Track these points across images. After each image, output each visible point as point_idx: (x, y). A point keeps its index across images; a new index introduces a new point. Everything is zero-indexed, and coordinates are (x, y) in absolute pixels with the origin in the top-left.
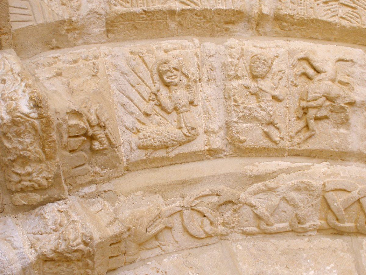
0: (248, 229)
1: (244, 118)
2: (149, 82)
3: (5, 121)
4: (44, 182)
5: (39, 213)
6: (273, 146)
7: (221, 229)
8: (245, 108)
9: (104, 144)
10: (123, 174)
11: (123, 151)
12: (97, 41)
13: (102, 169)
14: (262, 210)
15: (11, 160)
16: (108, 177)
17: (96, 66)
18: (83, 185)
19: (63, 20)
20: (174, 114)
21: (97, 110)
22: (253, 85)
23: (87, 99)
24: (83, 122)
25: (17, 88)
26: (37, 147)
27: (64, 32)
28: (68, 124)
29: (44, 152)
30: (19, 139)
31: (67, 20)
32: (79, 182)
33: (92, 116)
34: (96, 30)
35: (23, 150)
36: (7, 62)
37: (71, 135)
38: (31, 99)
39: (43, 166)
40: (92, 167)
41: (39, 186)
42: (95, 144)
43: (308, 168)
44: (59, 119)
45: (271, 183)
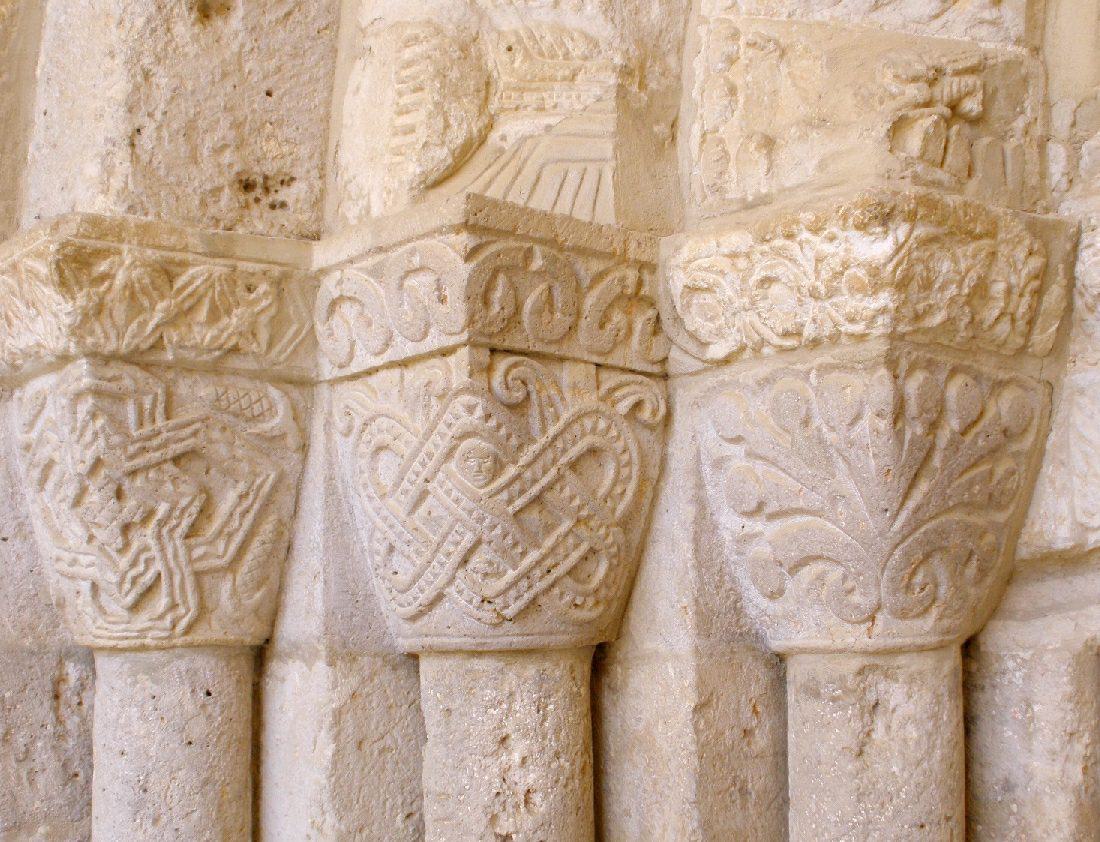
3: (891, 306)
4: (1036, 263)
5: (1090, 300)
9: (975, 86)
10: (1044, 63)
11: (991, 46)
12: (682, 18)
13: (1022, 112)
15: (970, 323)
16: (1043, 104)
17: (759, 41)
18: (1043, 175)
19: (618, 91)
21: (896, 76)
23: (862, 90)
24: (918, 118)
25: (810, 255)
26: (965, 248)
27: (644, 97)
28: (918, 158)
29: (979, 237)
30: (936, 286)
31: (620, 81)
32: (1033, 181)
33: (907, 92)
35: (960, 286)
36: (704, 262)
37: (939, 159)
38: (862, 227)
39: (1003, 250)
40: (1012, 136)
41: (1036, 277)
42: (968, 109)
44: (902, 175)
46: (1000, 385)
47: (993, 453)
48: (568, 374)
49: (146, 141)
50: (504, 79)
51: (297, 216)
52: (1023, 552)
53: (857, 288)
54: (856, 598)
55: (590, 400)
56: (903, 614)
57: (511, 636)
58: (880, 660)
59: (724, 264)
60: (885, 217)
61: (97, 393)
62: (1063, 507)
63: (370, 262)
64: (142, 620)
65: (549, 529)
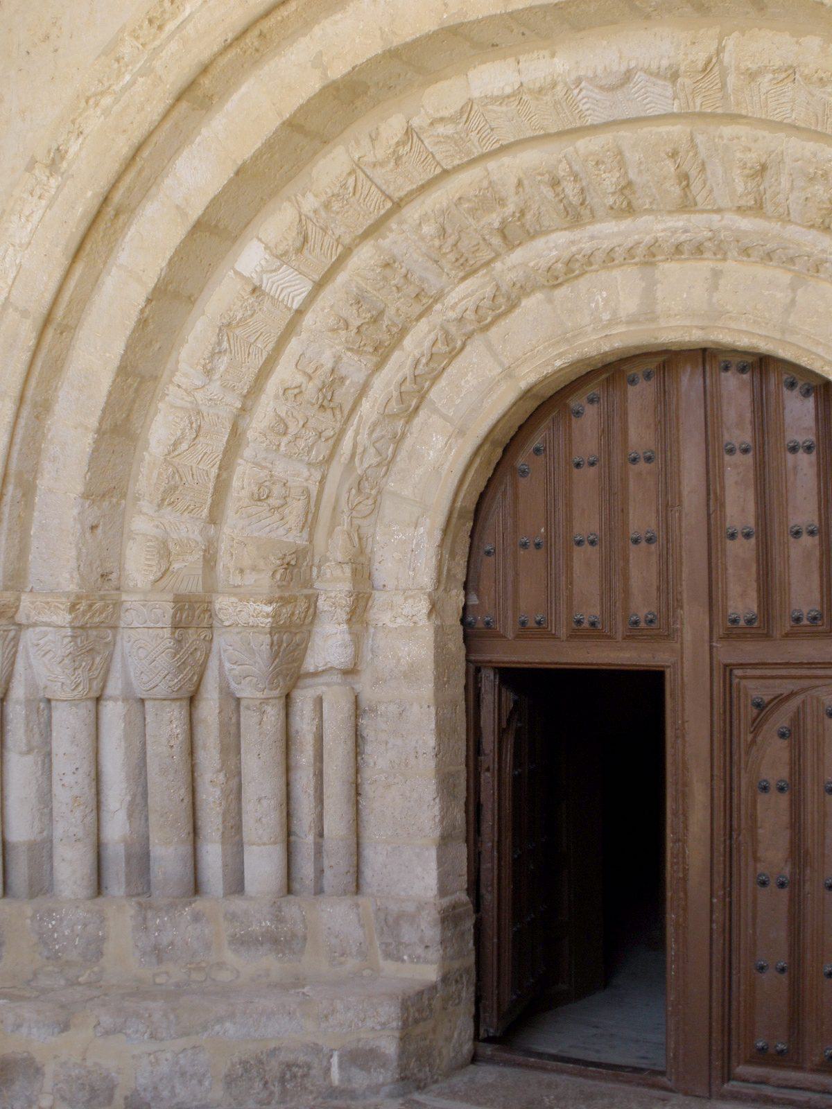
0: (382, 474)
1: (309, 452)
2: (261, 509)
6: (335, 438)
7: (374, 492)
8: (303, 449)
14: (374, 461)
18: (311, 575)
20: (288, 499)
22: (289, 437)
34: (212, 532)
38: (266, 604)
43: (361, 416)
45: (360, 450)
46: (296, 634)
47: (294, 650)
48: (190, 631)
49: (82, 569)
50: (174, 552)
51: (114, 583)
52: (302, 672)
53: (263, 616)
54: (259, 686)
55: (195, 637)
56: (271, 690)
57: (174, 696)
58: (266, 701)
59: (230, 605)
60: (271, 603)
61: (72, 636)
62: (312, 662)
63: (142, 603)
64: (76, 693)
65: (185, 669)
